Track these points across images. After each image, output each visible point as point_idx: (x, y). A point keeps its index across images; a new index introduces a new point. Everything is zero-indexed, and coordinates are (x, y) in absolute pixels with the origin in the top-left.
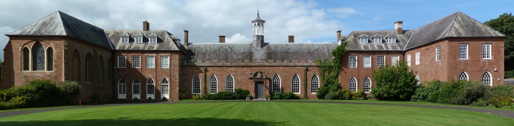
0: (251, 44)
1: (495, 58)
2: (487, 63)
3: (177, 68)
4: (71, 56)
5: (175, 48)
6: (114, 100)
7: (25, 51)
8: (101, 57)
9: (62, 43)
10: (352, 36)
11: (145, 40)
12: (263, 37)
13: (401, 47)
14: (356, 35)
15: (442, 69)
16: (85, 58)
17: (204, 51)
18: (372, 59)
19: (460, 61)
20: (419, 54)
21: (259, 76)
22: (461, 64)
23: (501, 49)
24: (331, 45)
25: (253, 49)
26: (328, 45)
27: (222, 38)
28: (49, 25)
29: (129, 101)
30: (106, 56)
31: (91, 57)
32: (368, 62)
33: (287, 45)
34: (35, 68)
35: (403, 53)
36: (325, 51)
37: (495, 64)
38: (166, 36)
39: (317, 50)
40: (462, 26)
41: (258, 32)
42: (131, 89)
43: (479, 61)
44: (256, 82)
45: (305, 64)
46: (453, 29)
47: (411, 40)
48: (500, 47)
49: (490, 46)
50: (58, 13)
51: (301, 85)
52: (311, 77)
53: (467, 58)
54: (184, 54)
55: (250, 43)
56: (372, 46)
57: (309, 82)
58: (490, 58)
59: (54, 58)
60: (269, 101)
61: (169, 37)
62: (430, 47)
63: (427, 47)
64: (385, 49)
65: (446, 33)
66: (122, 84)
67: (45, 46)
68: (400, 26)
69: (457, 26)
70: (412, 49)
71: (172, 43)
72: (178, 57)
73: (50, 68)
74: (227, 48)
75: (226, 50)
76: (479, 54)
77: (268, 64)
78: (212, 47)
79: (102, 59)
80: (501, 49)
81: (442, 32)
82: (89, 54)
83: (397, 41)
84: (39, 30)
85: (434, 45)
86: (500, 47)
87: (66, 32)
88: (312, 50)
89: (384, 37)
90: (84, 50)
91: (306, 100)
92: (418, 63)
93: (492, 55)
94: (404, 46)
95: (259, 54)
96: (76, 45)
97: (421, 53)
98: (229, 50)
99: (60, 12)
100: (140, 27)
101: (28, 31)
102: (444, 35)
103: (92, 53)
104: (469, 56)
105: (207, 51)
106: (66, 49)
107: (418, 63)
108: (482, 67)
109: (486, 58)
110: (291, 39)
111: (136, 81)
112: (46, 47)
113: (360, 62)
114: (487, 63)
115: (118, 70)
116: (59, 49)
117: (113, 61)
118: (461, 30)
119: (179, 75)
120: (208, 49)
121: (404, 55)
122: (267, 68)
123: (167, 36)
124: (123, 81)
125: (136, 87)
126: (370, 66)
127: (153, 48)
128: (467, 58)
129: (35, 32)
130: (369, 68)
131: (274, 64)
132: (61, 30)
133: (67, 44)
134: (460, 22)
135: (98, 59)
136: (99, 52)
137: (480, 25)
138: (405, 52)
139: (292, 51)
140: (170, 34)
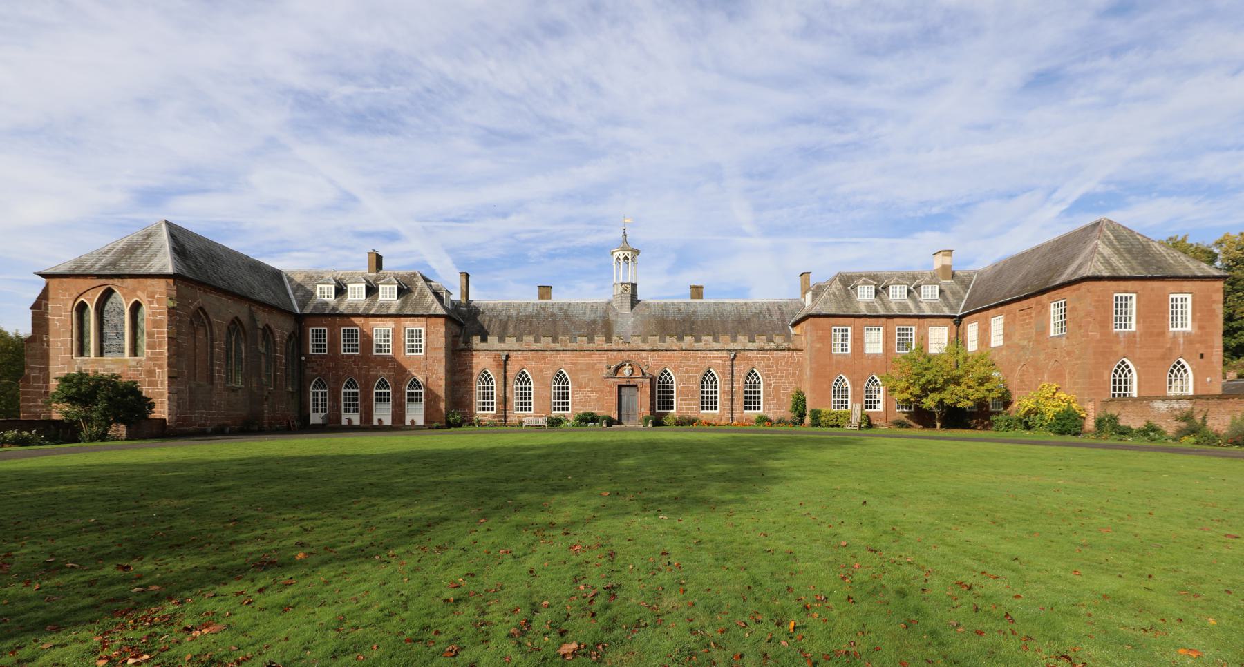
0: (609, 303)
1: (1201, 328)
2: (1181, 340)
3: (441, 354)
4: (187, 323)
5: (441, 311)
6: (303, 426)
7: (525, 405)
8: (267, 330)
9: (161, 286)
10: (837, 284)
11: (371, 290)
12: (634, 286)
13: (951, 308)
14: (848, 282)
15: (1069, 353)
16: (225, 330)
17: (503, 317)
18: (886, 333)
19: (1117, 334)
20: (1002, 321)
21: (626, 371)
22: (1118, 343)
23: (1215, 306)
24: (787, 304)
25: (611, 315)
26: (780, 305)
27: (545, 291)
28: (139, 251)
29: (332, 426)
30: (282, 328)
31: (242, 326)
32: (874, 342)
33: (688, 304)
34: (101, 352)
35: (958, 320)
36: (775, 318)
37: (1200, 342)
38: (419, 284)
39: (756, 315)
40: (1117, 251)
41: (625, 277)
42: (339, 402)
43: (1162, 334)
44: (620, 387)
45: (732, 346)
46: (1097, 257)
47: (974, 291)
48: (1214, 302)
49: (1189, 297)
50: (164, 226)
51: (723, 392)
52: (744, 375)
53: (1134, 328)
54: (460, 325)
55: (606, 300)
56: (885, 305)
57: (739, 385)
58: (1189, 328)
59: (145, 325)
60: (649, 430)
61: (425, 286)
62: (1033, 300)
63: (1024, 303)
64: (915, 312)
65: (1079, 267)
66: (319, 391)
67: (122, 300)
68: (947, 261)
69: (1106, 251)
70: (982, 306)
71: (431, 297)
72: (443, 330)
73: (134, 351)
74: (555, 310)
75: (553, 315)
76: (1164, 317)
77: (647, 346)
78: (522, 309)
79: (272, 332)
80: (1215, 306)
81: (1066, 267)
82: (236, 321)
83: (941, 291)
84: (114, 264)
85: (1045, 297)
86: (1214, 302)
87: (175, 266)
88: (745, 314)
89: (913, 284)
90: (223, 311)
91: (504, 428)
92: (997, 340)
93: (1193, 320)
94: (958, 305)
95: (626, 320)
96: (201, 298)
97: (1006, 318)
98: (560, 315)
99: (167, 223)
100: (363, 267)
101: (88, 264)
102: (1075, 272)
103: (245, 319)
104: (1138, 322)
105: (510, 317)
106: (171, 304)
107: (997, 340)
108: (1170, 349)
109: (1179, 328)
110: (697, 292)
111: (351, 384)
112: (127, 300)
113: (858, 341)
114: (1181, 340)
115: (309, 358)
116: (156, 305)
117: (298, 339)
118: (1115, 260)
119: (447, 371)
120: (513, 313)
121: (958, 325)
122: (644, 354)
123: (421, 283)
124: (320, 384)
125: (351, 398)
126: (881, 351)
127: (389, 308)
128: (1134, 328)
129: (104, 267)
130: (877, 355)
131: (660, 345)
132: (165, 262)
133: (174, 293)
134: (1111, 242)
135: (260, 332)
136: (263, 318)
137: (1162, 249)
138: (961, 317)
139: (701, 315)
140: (426, 280)
